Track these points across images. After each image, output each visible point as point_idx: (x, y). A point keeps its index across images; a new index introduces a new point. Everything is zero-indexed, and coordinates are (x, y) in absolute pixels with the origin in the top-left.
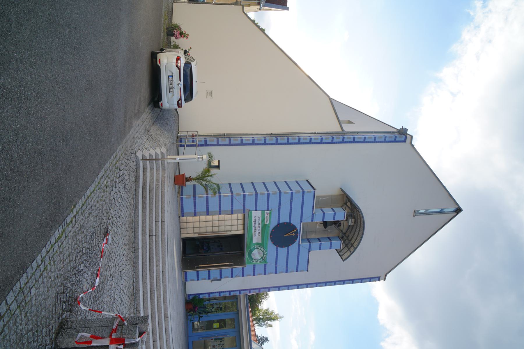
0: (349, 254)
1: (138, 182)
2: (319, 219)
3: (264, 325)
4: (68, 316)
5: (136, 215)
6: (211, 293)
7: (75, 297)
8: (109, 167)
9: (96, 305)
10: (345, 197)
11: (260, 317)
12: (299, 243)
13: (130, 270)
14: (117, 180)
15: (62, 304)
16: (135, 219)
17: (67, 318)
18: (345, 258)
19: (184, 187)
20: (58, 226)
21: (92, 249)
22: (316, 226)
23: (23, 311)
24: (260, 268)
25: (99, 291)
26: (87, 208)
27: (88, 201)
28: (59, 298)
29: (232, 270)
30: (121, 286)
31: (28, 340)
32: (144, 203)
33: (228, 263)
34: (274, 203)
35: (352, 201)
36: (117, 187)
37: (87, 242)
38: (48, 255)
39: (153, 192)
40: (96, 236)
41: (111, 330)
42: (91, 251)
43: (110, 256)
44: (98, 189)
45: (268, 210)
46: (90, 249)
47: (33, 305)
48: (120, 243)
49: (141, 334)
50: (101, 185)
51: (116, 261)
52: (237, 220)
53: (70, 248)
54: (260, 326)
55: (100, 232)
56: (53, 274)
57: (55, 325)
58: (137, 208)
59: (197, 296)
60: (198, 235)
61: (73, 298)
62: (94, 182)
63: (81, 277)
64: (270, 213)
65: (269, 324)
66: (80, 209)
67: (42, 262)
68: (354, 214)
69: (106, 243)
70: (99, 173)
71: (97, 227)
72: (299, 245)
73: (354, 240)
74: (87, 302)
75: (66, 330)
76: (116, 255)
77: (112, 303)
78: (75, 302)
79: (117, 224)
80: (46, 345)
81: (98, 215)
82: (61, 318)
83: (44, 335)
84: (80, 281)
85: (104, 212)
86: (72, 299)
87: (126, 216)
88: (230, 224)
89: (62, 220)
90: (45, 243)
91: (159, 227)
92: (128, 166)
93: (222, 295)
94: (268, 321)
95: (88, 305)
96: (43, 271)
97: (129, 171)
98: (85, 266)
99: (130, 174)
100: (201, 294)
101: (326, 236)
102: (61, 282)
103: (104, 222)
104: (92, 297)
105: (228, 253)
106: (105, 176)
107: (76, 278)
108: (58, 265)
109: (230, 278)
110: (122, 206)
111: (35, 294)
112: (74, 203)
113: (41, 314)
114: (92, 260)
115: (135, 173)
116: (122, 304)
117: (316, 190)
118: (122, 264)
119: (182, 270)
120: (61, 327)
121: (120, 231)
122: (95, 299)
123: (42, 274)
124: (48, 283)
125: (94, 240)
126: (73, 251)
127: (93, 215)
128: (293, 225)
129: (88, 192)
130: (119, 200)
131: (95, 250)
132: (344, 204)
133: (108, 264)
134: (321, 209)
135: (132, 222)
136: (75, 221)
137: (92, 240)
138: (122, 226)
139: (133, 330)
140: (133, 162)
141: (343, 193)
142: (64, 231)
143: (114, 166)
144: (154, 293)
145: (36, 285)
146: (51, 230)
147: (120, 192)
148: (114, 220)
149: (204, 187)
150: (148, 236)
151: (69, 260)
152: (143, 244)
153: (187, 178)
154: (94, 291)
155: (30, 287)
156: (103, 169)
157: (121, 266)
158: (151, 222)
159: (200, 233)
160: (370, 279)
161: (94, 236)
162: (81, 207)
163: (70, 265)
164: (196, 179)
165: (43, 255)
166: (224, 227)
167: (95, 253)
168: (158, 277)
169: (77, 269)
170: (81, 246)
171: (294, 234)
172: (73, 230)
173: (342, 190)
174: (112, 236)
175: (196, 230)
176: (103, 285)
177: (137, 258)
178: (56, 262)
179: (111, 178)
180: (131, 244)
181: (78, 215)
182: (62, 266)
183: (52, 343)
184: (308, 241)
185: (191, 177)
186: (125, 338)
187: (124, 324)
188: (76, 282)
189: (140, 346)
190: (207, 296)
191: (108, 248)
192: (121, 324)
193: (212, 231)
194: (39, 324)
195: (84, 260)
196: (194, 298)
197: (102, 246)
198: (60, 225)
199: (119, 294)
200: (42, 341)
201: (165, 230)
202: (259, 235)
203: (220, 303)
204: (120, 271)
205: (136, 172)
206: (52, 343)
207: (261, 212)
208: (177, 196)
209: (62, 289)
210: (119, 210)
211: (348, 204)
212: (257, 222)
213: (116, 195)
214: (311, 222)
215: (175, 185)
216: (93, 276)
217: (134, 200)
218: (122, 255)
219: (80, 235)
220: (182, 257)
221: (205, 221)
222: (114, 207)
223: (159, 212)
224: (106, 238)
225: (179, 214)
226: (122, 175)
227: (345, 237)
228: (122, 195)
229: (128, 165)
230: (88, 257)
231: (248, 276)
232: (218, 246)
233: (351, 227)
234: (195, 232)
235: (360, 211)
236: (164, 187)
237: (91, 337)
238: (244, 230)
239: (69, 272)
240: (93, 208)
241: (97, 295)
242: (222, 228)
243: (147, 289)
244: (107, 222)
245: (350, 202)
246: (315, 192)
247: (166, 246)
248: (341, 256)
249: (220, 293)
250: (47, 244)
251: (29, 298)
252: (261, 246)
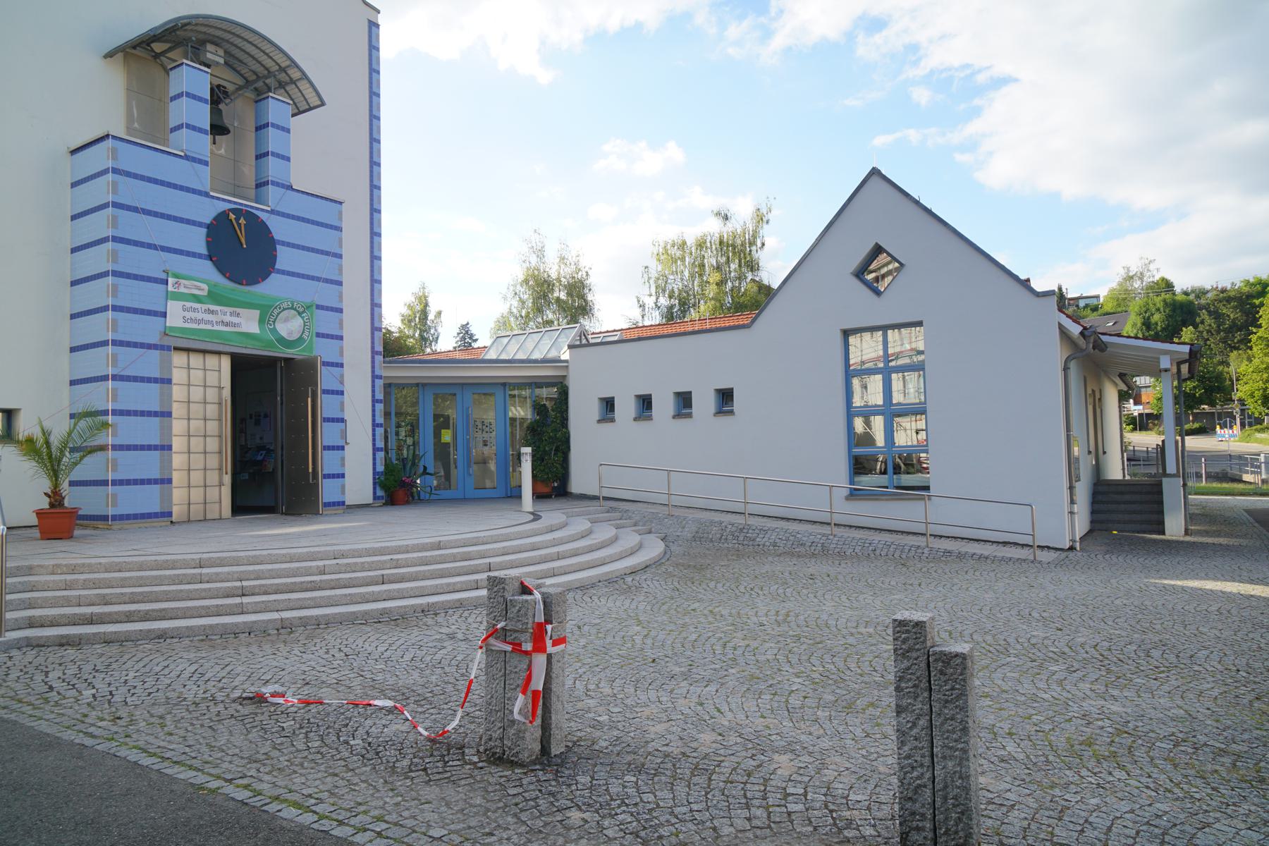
0: (308, 85)
1: (80, 639)
2: (203, 144)
3: (436, 330)
4: (473, 751)
5: (187, 634)
6: (374, 445)
7: (429, 743)
8: (48, 720)
9: (436, 698)
10: (133, 51)
11: (417, 335)
12: (267, 211)
13: (339, 633)
14: (88, 693)
15: (451, 768)
16: (198, 636)
17: (478, 751)
18: (316, 98)
19: (80, 513)
20: (265, 816)
21: (308, 727)
22: (221, 156)
23: (482, 842)
24: (325, 322)
25: (403, 695)
26: (195, 758)
27: (175, 759)
28: (438, 777)
29: (325, 392)
30: (381, 649)
31: (537, 817)
32: (146, 617)
33: (309, 400)
34: (150, 263)
35: (152, 34)
36: (111, 692)
37: (292, 741)
38: (346, 821)
39: (111, 594)
40: (270, 722)
41: (514, 655)
42: (313, 729)
43: (312, 682)
44: (128, 739)
45: (167, 281)
46: (307, 732)
47: (465, 826)
48: (274, 663)
49: (525, 590)
50: (116, 733)
51: (323, 669)
52: (189, 368)
53: (316, 776)
54: (437, 338)
55: (256, 714)
56: (388, 800)
57: (496, 773)
58: (166, 633)
60: (226, 473)
61: (432, 748)
62: (112, 751)
63: (381, 739)
64: (176, 276)
65: (435, 316)
66: (204, 773)
67: (368, 830)
68: (194, 39)
69: (283, 696)
70: (79, 744)
71: (244, 725)
72: (272, 212)
73: (270, 60)
74: (434, 716)
75: (506, 749)
76: (307, 669)
77: (424, 666)
78: (440, 743)
79: (223, 678)
80: (539, 781)
81: (210, 727)
82: (480, 765)
83: (521, 790)
84: (391, 740)
85: (197, 714)
86: (436, 750)
87: (195, 659)
88: (202, 388)
89: (247, 809)
90: (319, 833)
91: (217, 574)
92: (31, 669)
93: (380, 420)
94: (429, 318)
95: (439, 714)
96: (387, 822)
97: (47, 667)
98: (353, 735)
99: (57, 662)
100: (374, 468)
101: (251, 136)
102: (401, 780)
103: (226, 709)
104: (420, 710)
105: (279, 398)
106: (81, 727)
107: (386, 750)
108: (364, 794)
110: (166, 671)
111: (443, 827)
112: (190, 790)
113: (480, 805)
114: (335, 723)
115: (50, 649)
116: (420, 643)
117: (111, 133)
118: (327, 653)
119: (317, 513)
120: (498, 759)
121: (240, 668)
122: (423, 703)
123: (396, 824)
124: (411, 806)
125: (282, 725)
126: (322, 768)
127: (213, 739)
128: (215, 219)
129: (146, 761)
130: (150, 681)
131: (309, 720)
132: (158, 60)
133: (335, 686)
134: (171, 132)
135: (208, 643)
136: (240, 778)
137: (283, 729)
138: (227, 666)
139: (517, 608)
140: (10, 658)
141: (120, 56)
142: (277, 798)
143: (40, 708)
144: (387, 575)
145: (423, 830)
146: (282, 828)
147: (126, 682)
148: (214, 686)
149: (84, 456)
150: (243, 598)
151: (347, 772)
152: (268, 609)
153: (52, 505)
154: (405, 706)
155: (431, 839)
156: (59, 735)
157: (333, 656)
158: (203, 594)
159: (220, 469)
160: (373, 48)
161: (273, 728)
162: (199, 770)
163: (358, 767)
164: (56, 480)
165: (349, 831)
166: (207, 405)
167: (314, 717)
168: (349, 569)
169: (364, 752)
170: (306, 753)
171: (242, 221)
172: (267, 778)
173: (110, 55)
174: (260, 685)
175: (213, 477)
176: (387, 689)
177: (304, 622)
178: (359, 800)
179: (85, 710)
180: (269, 638)
181: (222, 775)
182: (365, 785)
183: (533, 770)
184: (264, 185)
185: (49, 491)
186: (534, 622)
187: (503, 629)
188: (395, 749)
189: (551, 590)
190: (381, 455)
191: (294, 690)
192: (502, 635)
193: (217, 439)
194: (501, 804)
195: (339, 740)
196: (384, 486)
197: (292, 706)
198: (264, 811)
199: (400, 653)
200: (534, 790)
201: (226, 558)
202: (239, 314)
203: (397, 427)
204: (346, 655)
205: (44, 646)
206: (533, 770)
207: (170, 303)
208: (108, 532)
209: (417, 773)
210: (182, 676)
211: (158, 47)
212: (200, 316)
213: (136, 691)
214: (209, 168)
215: (72, 537)
216: (372, 714)
217: (138, 643)
218: (304, 656)
219: (275, 761)
220: (282, 513)
221: (186, 455)
222: (174, 690)
223: (174, 575)
224: (271, 699)
225: (164, 524)
226: (66, 684)
227: (256, 85)
228: (132, 674)
229: (25, 670)
230: (329, 733)
231: (341, 354)
232: (257, 423)
233: (232, 61)
234: (217, 483)
235: (185, 21)
236: (90, 565)
237: (524, 692)
238: (219, 353)
239: (375, 768)
240: (191, 743)
241: (413, 698)
242: (212, 410)
243: (379, 592)
244: (222, 702)
245: (152, 42)
246: (114, 137)
247: (269, 552)
248: (310, 109)
249: (375, 425)
250: (321, 829)
251: (454, 837)
252: (267, 314)
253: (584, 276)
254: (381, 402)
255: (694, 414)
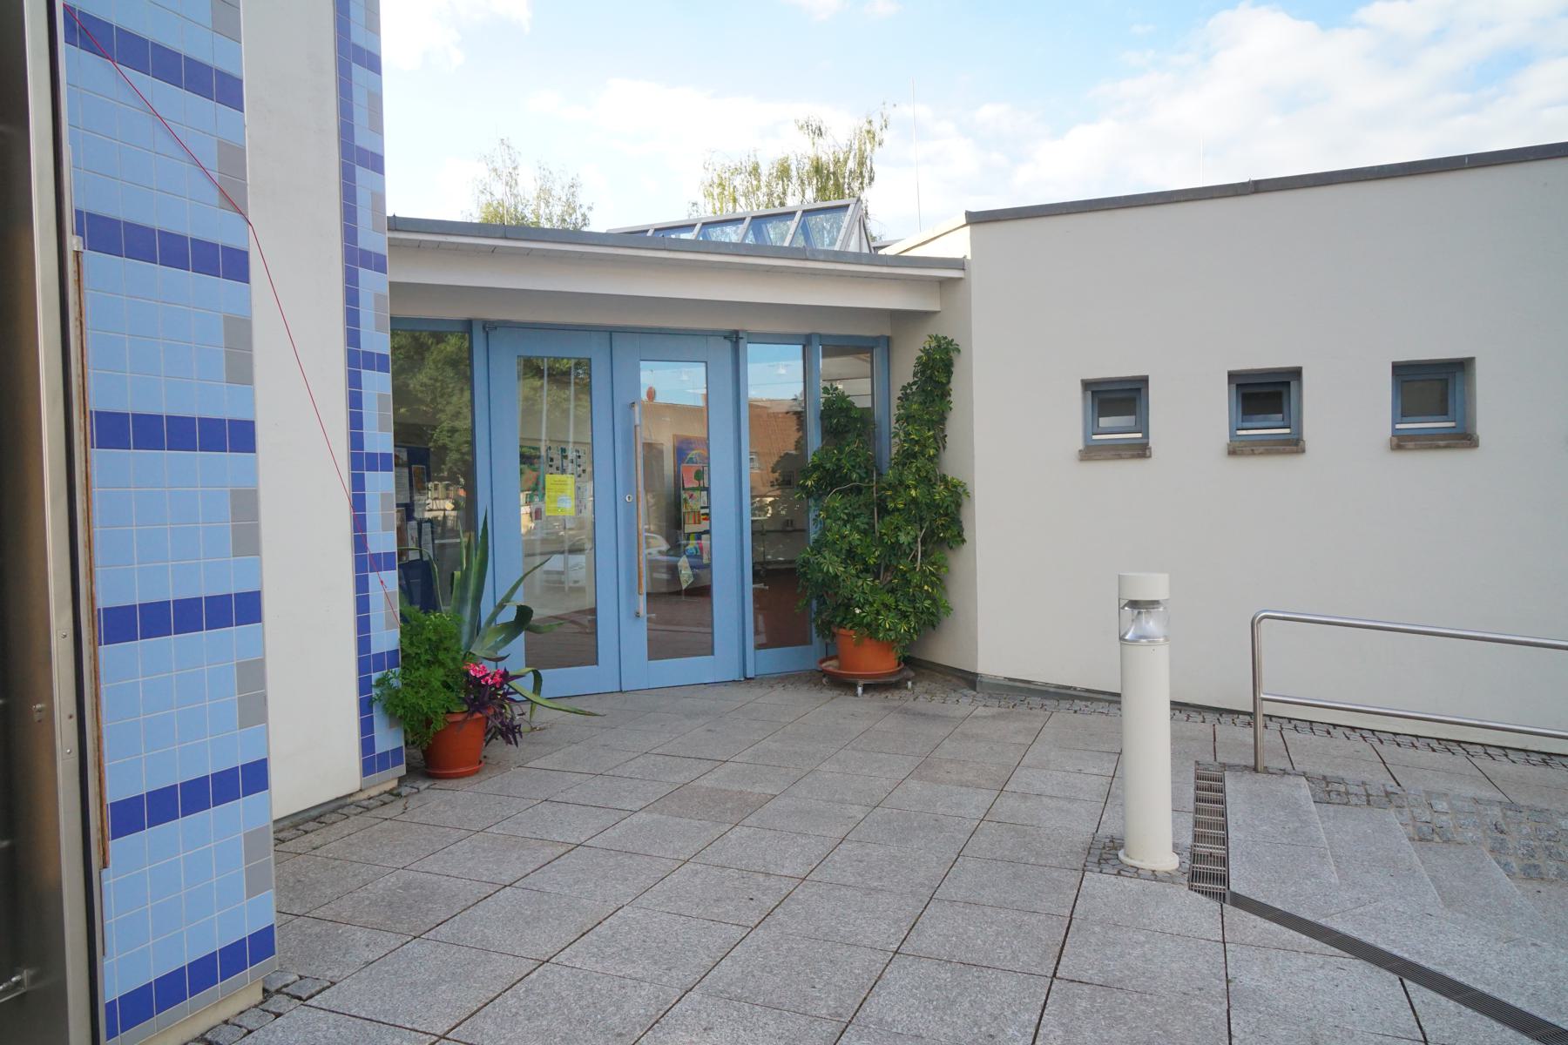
59: (380, 683)
100: (363, 643)
109: (253, 473)
253: (579, 221)
254: (382, 368)
255: (1074, 404)
